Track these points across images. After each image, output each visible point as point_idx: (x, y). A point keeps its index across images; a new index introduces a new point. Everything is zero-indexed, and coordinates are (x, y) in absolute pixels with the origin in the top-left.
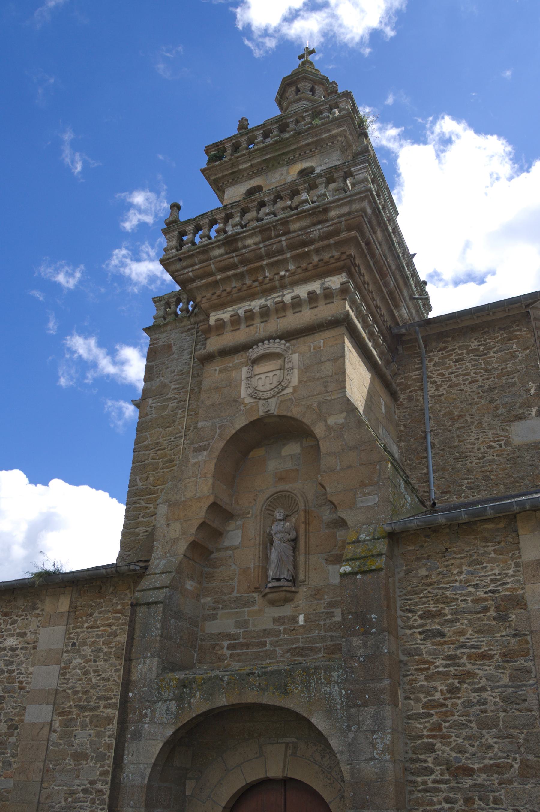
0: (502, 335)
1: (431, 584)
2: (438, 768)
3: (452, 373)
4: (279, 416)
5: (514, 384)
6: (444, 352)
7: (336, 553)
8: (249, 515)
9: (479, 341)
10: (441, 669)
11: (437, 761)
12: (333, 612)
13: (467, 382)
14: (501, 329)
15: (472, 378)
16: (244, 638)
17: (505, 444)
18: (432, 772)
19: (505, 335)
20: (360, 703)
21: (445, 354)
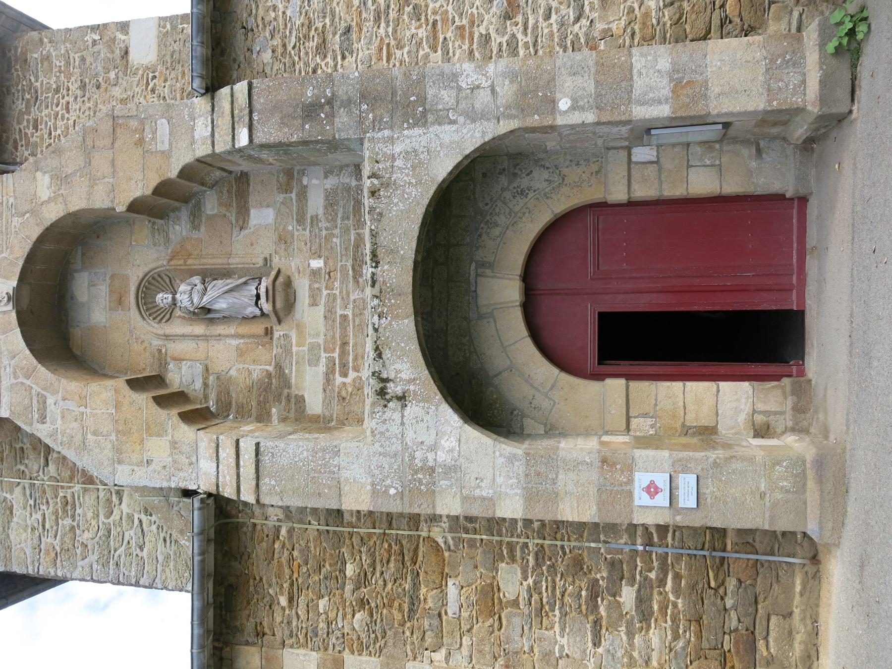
0: (16, 70)
1: (284, 45)
2: (509, 29)
3: (50, 134)
4: (21, 279)
5: (83, 59)
6: (20, 144)
7: (234, 215)
8: (164, 351)
9: (18, 99)
10: (390, 30)
11: (501, 31)
12: (312, 217)
13: (67, 115)
14: (9, 71)
15: (62, 110)
16: (333, 351)
17: (153, 72)
18: (513, 36)
19: (18, 67)
20: (420, 109)
21: (23, 142)
